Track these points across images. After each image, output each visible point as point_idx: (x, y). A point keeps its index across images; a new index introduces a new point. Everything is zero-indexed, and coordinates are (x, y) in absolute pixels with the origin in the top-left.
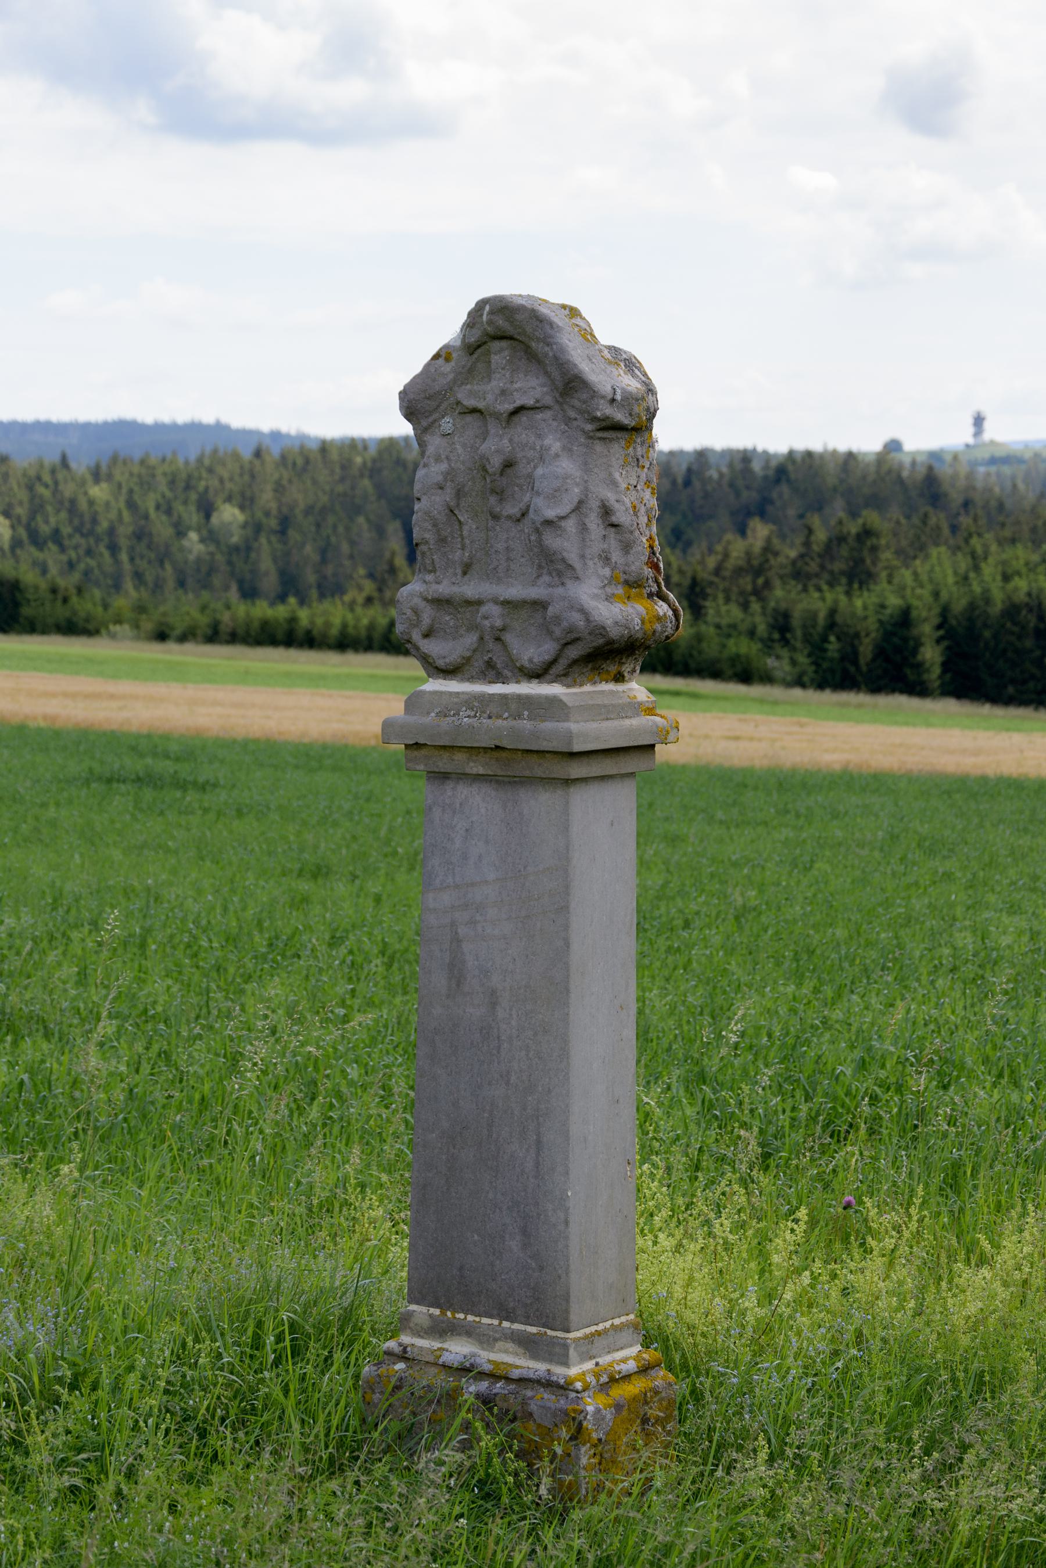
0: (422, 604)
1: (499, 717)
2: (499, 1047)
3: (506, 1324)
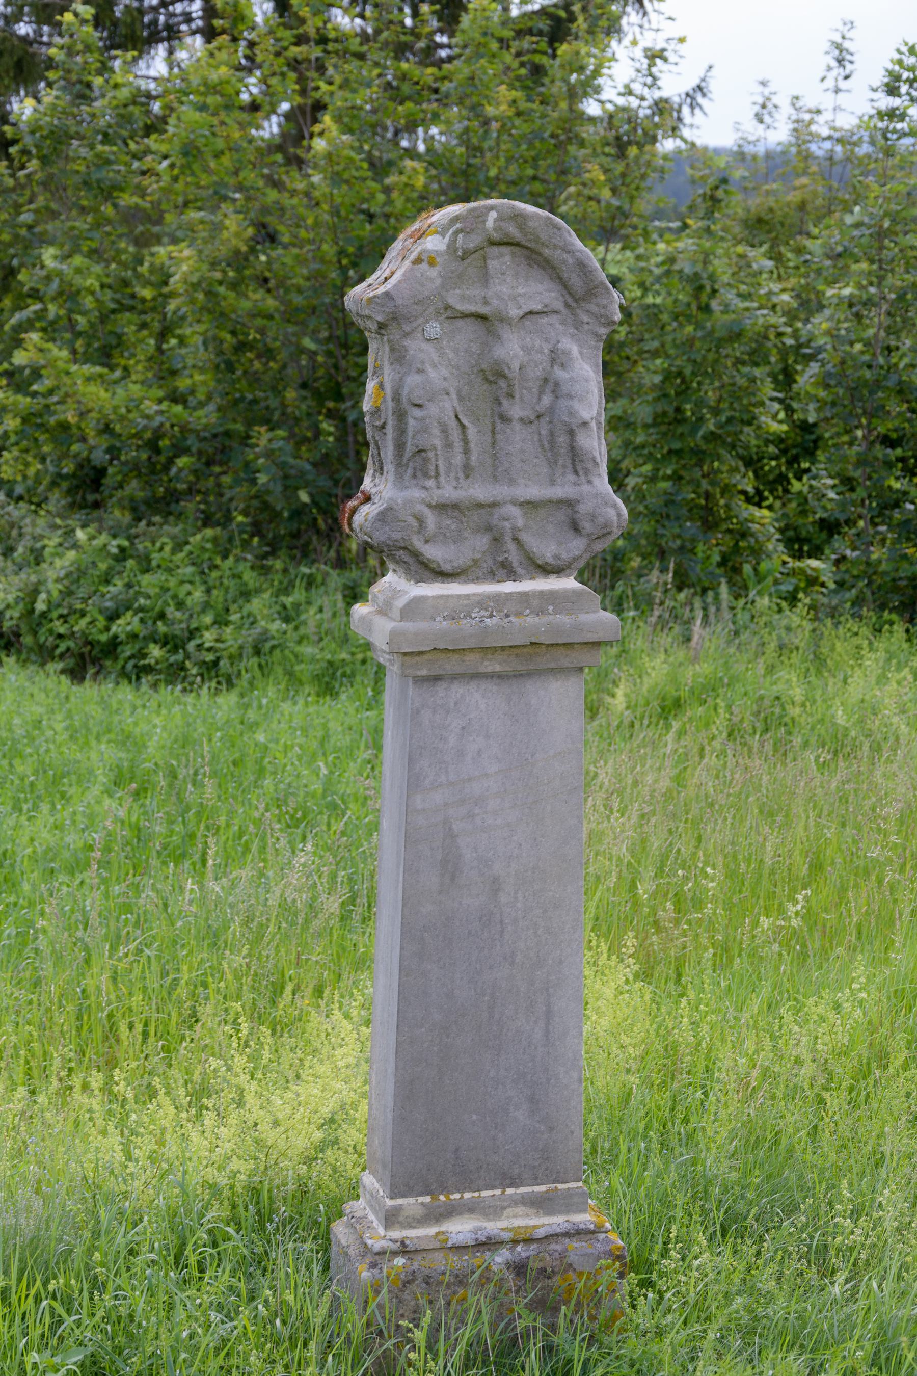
0: (427, 512)
1: (518, 614)
2: (502, 931)
3: (509, 1191)
